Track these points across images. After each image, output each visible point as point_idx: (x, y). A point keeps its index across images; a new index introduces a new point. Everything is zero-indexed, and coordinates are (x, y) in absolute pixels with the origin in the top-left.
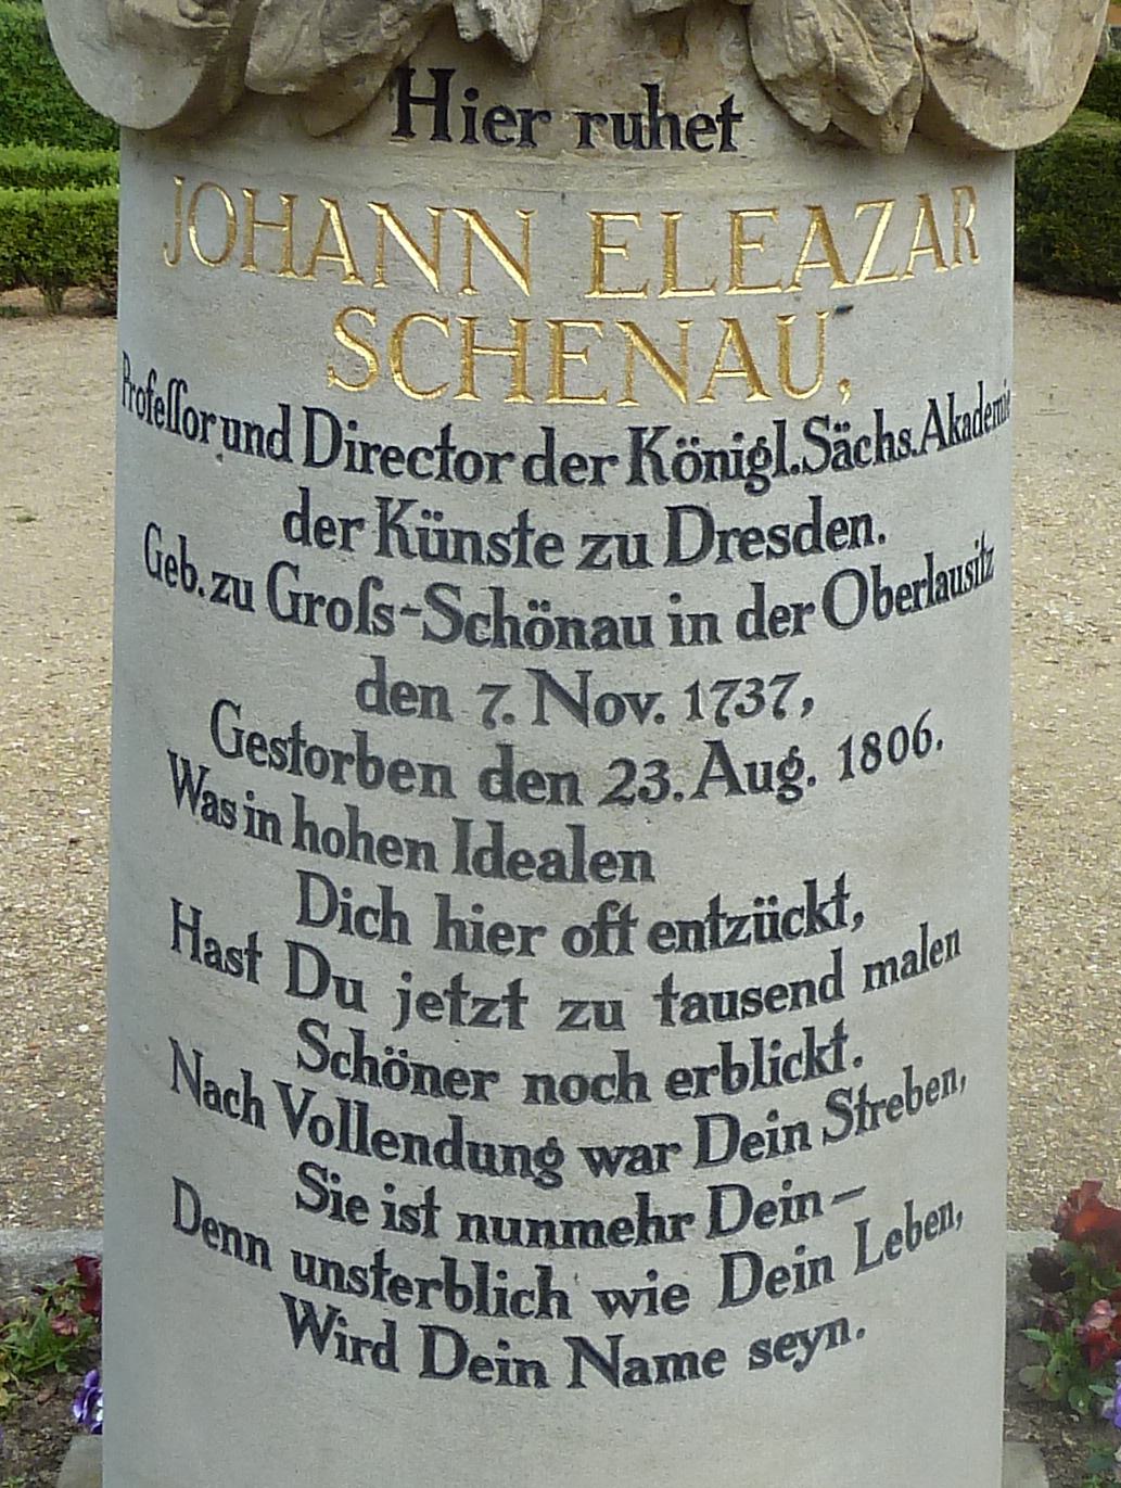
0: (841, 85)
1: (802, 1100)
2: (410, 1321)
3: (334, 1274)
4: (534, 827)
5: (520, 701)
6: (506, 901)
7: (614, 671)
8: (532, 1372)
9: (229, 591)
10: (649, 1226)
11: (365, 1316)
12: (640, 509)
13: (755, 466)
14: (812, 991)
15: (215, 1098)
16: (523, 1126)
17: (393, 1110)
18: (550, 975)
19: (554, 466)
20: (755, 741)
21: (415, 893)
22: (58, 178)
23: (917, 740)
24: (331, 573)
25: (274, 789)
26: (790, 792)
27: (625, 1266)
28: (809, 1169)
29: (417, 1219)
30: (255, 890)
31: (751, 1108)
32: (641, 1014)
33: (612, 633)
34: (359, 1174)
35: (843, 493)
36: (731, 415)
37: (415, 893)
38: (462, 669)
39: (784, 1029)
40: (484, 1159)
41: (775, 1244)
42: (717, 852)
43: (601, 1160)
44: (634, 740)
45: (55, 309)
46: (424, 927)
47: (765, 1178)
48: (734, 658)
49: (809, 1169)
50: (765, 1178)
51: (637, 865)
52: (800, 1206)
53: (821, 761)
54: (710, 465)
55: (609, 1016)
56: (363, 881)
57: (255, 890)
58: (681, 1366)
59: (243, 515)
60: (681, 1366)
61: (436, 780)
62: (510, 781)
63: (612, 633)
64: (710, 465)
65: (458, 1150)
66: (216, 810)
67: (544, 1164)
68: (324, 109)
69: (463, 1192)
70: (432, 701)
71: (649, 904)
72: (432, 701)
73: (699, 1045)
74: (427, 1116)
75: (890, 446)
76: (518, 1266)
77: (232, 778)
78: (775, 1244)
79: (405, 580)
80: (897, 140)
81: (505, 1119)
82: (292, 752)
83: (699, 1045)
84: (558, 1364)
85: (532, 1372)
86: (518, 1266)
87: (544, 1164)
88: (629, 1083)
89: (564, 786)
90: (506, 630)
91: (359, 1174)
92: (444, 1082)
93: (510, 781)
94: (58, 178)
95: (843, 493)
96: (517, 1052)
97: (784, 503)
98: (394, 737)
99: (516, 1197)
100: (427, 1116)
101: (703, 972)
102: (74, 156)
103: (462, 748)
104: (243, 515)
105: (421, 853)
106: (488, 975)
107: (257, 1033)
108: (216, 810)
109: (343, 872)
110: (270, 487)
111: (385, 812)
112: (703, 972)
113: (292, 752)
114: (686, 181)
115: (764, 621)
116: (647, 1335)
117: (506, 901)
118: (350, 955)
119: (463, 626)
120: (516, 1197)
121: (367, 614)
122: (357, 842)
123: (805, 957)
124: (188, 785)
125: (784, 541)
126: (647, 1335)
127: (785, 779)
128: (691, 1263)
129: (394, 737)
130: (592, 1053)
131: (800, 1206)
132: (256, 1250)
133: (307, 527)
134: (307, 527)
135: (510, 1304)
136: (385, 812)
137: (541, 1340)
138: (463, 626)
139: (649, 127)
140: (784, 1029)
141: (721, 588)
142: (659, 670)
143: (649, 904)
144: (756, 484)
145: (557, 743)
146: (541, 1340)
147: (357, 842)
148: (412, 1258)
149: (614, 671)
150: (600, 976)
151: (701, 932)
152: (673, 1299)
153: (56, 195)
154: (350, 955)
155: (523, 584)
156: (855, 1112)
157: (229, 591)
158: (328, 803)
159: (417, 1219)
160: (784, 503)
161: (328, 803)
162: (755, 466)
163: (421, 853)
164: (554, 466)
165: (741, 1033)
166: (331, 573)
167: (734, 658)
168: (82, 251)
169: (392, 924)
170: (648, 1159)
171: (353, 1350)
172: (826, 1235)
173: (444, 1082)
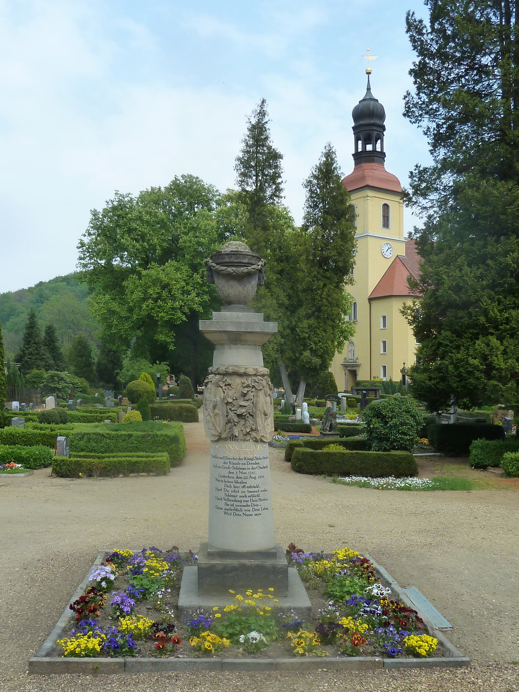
0: (256, 438)
1: (257, 498)
2: (232, 512)
3: (227, 510)
4: (239, 480)
5: (238, 473)
6: (238, 485)
7: (244, 471)
8: (240, 515)
9: (220, 467)
10: (247, 506)
11: (229, 512)
12: (245, 462)
13: (252, 460)
14: (257, 491)
15: (219, 499)
16: (240, 499)
17: (231, 498)
18: (241, 489)
19: (240, 459)
20: (253, 476)
21: (232, 485)
22: (147, 457)
23: (263, 477)
24: (227, 466)
25: (223, 479)
26: (255, 479)
27: (246, 508)
28: (258, 503)
29: (232, 505)
30: (221, 485)
31: (254, 499)
32: (246, 492)
33: (243, 469)
34: (229, 503)
35: (257, 461)
36: (251, 456)
37: (232, 485)
38: (235, 471)
39: (256, 494)
40: (237, 501)
41: (256, 508)
42: (250, 482)
43: (244, 501)
44: (245, 475)
45: (149, 475)
46: (233, 487)
47: (255, 503)
48: (251, 471)
49: (258, 503)
50: (255, 503)
51: (246, 483)
52: (257, 505)
53: (257, 477)
54: (249, 459)
55: (244, 492)
56: (229, 484)
57: (221, 485)
58: (250, 515)
59: (220, 463)
60: (250, 515)
61: (233, 478)
62: (237, 478)
63: (243, 469)
64: (249, 459)
65: (235, 501)
66: (219, 481)
67: (241, 501)
68: (226, 439)
69: (236, 503)
70: (233, 473)
71: (247, 485)
72: (233, 473)
73: (250, 494)
74: (233, 499)
75: (260, 459)
76: (239, 508)
77: (220, 479)
78: (256, 508)
79: (231, 466)
80: (259, 441)
81: (238, 499)
82: (224, 477)
83: (250, 494)
84: (242, 515)
85: (240, 515)
86: (239, 508)
87: (241, 501)
88: (246, 496)
89: (241, 478)
90: (237, 469)
91: (229, 503)
92: (234, 496)
93: (237, 478)
94: (149, 457)
95: (257, 461)
96: (239, 494)
97: (254, 462)
98: (230, 475)
99: (239, 504)
100: (233, 499)
101: (250, 490)
102: (149, 454)
103: (235, 476)
104: (220, 463)
105: (232, 482)
106: (237, 490)
107: (222, 494)
108: (219, 481)
109: (227, 484)
110: (223, 461)
111: (230, 480)
112: (250, 490)
113: (224, 477)
114: (247, 443)
115: (253, 468)
116: (248, 513)
117: (238, 485)
118: (228, 489)
119: (235, 468)
120: (239, 504)
121: (229, 468)
122: (228, 482)
123: (257, 489)
124: (217, 480)
125: (254, 464)
126: (248, 513)
127: (255, 478)
128: (250, 508)
129: (230, 475)
130: (243, 494)
131: (257, 505)
132: (222, 509)
133: (225, 463)
134: (225, 463)
135: (239, 511)
136: (230, 480)
137: (241, 513)
138: (235, 468)
139: (245, 440)
140: (256, 494)
141: (250, 466)
142: (247, 471)
143: (247, 485)
144: (252, 460)
145: (240, 475)
146: (241, 513)
147: (228, 482)
148: (232, 508)
149: (244, 471)
150: (244, 490)
151: (250, 487)
152: (249, 510)
153: (149, 459)
154: (228, 489)
155: (238, 466)
156: (261, 500)
157: (220, 467)
158: (226, 479)
159: (232, 505)
160: (254, 462)
161: (226, 479)
162: (252, 460)
163: (232, 482)
164: (240, 459)
165: (253, 494)
166: (227, 466)
167: (251, 471)
168: (153, 467)
169: (231, 487)
170: (247, 501)
171: (229, 514)
172: (259, 508)
173: (234, 496)
